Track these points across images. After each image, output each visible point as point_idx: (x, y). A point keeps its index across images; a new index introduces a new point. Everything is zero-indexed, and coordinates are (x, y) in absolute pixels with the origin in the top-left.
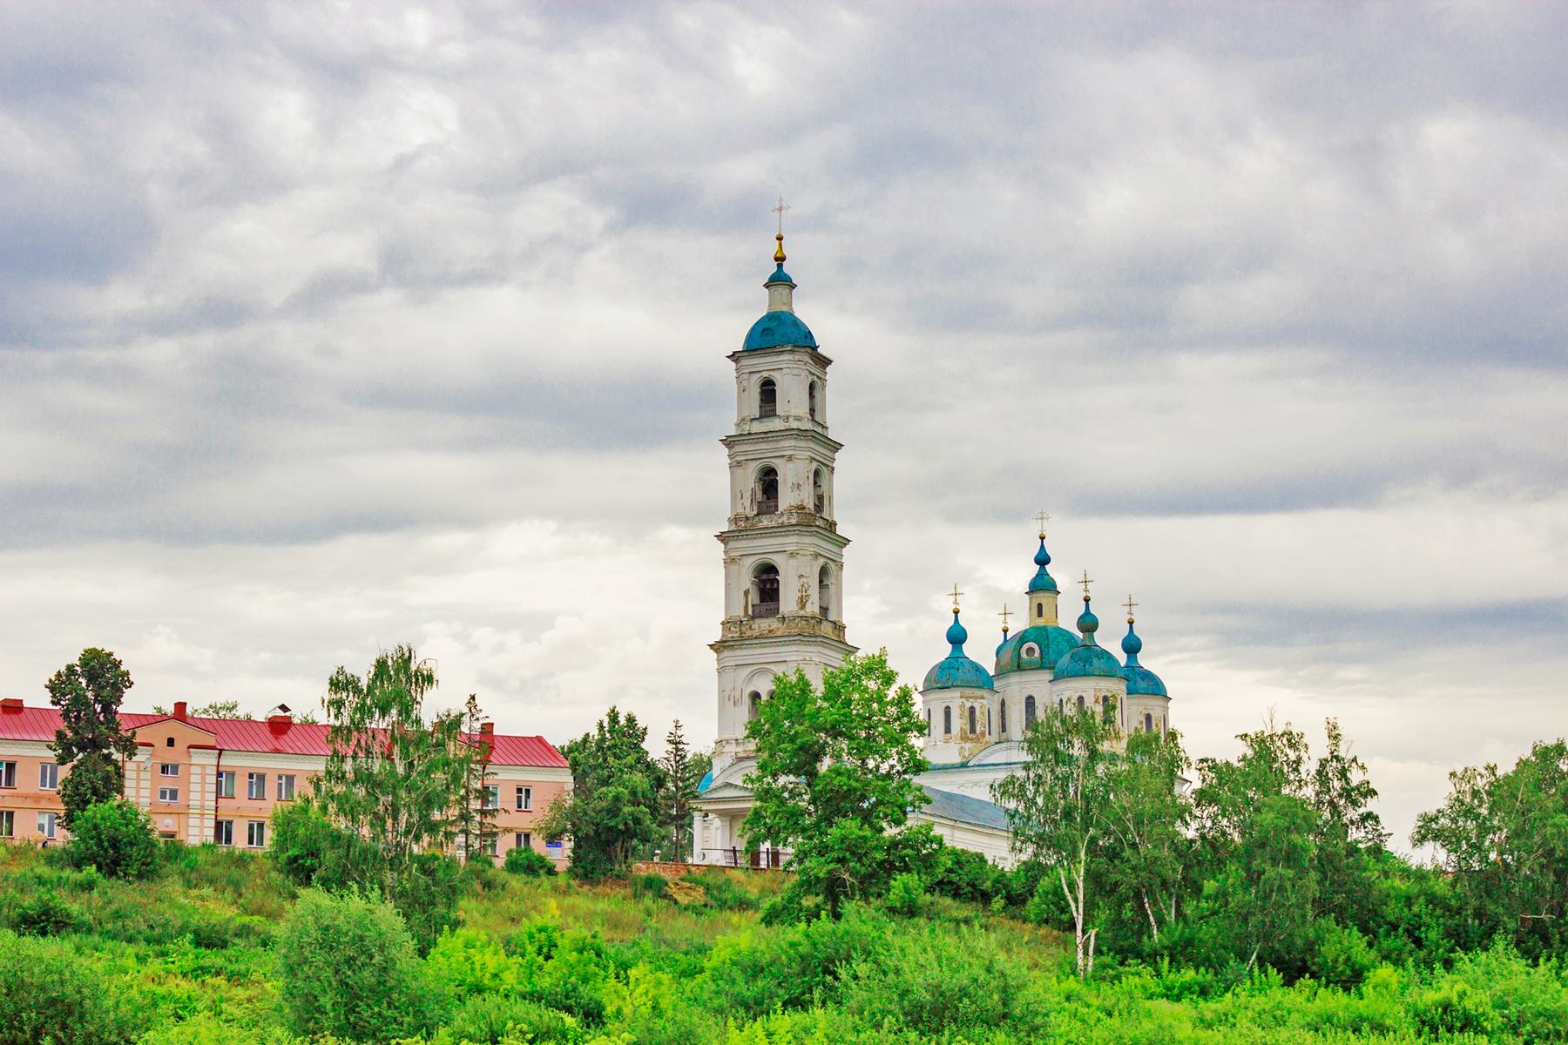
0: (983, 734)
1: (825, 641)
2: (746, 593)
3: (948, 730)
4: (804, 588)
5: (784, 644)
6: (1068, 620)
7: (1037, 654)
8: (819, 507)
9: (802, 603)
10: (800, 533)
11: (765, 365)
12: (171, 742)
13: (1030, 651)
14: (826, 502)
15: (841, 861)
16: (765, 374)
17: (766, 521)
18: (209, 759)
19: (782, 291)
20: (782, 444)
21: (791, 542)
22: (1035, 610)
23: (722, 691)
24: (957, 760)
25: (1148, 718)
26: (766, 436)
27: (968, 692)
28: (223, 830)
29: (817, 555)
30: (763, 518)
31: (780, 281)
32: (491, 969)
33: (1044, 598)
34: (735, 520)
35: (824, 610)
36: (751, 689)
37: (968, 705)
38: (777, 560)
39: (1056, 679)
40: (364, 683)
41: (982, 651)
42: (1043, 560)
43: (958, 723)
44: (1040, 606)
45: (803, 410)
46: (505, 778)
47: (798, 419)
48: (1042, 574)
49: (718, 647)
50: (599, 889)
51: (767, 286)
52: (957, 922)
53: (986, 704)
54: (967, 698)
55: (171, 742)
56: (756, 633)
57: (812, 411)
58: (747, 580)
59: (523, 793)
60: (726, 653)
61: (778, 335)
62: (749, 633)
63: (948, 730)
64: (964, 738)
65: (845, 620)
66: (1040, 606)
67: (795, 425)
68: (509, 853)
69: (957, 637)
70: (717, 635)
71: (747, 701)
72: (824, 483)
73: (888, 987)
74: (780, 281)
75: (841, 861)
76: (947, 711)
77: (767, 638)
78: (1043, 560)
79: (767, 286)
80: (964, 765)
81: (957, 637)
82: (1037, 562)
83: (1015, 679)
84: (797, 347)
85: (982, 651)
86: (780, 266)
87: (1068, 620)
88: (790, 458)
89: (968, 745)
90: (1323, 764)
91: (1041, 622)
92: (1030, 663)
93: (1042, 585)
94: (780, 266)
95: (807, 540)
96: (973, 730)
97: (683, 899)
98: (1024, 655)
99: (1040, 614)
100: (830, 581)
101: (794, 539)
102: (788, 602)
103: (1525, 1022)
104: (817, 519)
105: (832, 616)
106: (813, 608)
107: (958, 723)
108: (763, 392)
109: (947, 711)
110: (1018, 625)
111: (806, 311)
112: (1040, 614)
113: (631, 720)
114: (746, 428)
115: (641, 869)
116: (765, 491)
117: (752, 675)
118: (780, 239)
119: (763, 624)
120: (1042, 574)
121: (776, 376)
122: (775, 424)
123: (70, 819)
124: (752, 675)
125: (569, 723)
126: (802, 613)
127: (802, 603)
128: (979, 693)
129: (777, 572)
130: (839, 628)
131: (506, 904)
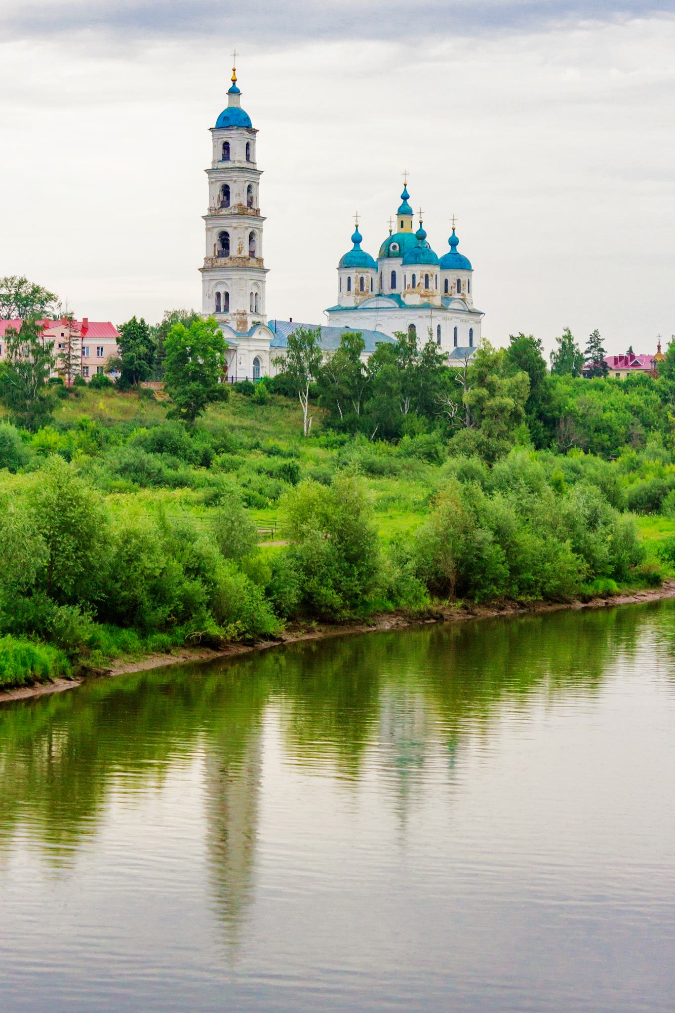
0: (367, 291)
1: (251, 269)
2: (215, 245)
3: (349, 289)
4: (241, 244)
5: (228, 271)
7: (398, 249)
8: (250, 203)
9: (240, 251)
10: (239, 218)
11: (226, 135)
13: (394, 247)
14: (254, 200)
15: (191, 398)
16: (225, 140)
17: (224, 211)
19: (235, 97)
20: (232, 174)
21: (235, 222)
23: (204, 291)
25: (459, 281)
26: (224, 170)
27: (360, 269)
29: (247, 228)
31: (234, 92)
32: (54, 441)
33: (404, 218)
34: (210, 210)
35: (252, 254)
37: (360, 276)
38: (229, 230)
40: (18, 331)
41: (372, 247)
42: (405, 197)
44: (402, 222)
45: (243, 158)
46: (91, 343)
47: (240, 162)
48: (405, 204)
49: (202, 270)
50: (126, 394)
52: (282, 406)
53: (369, 275)
54: (359, 273)
56: (219, 264)
57: (248, 156)
58: (215, 239)
59: (100, 350)
60: (205, 274)
61: (233, 121)
63: (349, 289)
64: (357, 294)
65: (264, 256)
66: (402, 222)
67: (238, 165)
68: (93, 376)
69: (357, 239)
71: (214, 296)
72: (253, 190)
74: (234, 92)
75: (191, 398)
76: (349, 279)
77: (223, 268)
78: (405, 197)
80: (356, 308)
81: (357, 239)
82: (402, 198)
83: (386, 261)
84: (239, 127)
85: (372, 247)
86: (234, 84)
88: (235, 181)
89: (359, 297)
90: (427, 345)
91: (402, 230)
94: (234, 84)
95: (242, 221)
96: (362, 289)
97: (159, 399)
98: (391, 249)
99: (402, 226)
100: (256, 238)
101: (235, 221)
102: (233, 251)
104: (250, 210)
105: (257, 255)
106: (246, 253)
107: (355, 286)
108: (224, 148)
109: (349, 279)
111: (245, 104)
112: (402, 226)
113: (142, 321)
114: (216, 166)
115: (144, 385)
116: (225, 195)
117: (217, 284)
119: (222, 260)
120: (405, 204)
121: (230, 141)
124: (217, 284)
125: (120, 320)
127: (240, 251)
128: (365, 270)
130: (260, 261)
131: (84, 404)
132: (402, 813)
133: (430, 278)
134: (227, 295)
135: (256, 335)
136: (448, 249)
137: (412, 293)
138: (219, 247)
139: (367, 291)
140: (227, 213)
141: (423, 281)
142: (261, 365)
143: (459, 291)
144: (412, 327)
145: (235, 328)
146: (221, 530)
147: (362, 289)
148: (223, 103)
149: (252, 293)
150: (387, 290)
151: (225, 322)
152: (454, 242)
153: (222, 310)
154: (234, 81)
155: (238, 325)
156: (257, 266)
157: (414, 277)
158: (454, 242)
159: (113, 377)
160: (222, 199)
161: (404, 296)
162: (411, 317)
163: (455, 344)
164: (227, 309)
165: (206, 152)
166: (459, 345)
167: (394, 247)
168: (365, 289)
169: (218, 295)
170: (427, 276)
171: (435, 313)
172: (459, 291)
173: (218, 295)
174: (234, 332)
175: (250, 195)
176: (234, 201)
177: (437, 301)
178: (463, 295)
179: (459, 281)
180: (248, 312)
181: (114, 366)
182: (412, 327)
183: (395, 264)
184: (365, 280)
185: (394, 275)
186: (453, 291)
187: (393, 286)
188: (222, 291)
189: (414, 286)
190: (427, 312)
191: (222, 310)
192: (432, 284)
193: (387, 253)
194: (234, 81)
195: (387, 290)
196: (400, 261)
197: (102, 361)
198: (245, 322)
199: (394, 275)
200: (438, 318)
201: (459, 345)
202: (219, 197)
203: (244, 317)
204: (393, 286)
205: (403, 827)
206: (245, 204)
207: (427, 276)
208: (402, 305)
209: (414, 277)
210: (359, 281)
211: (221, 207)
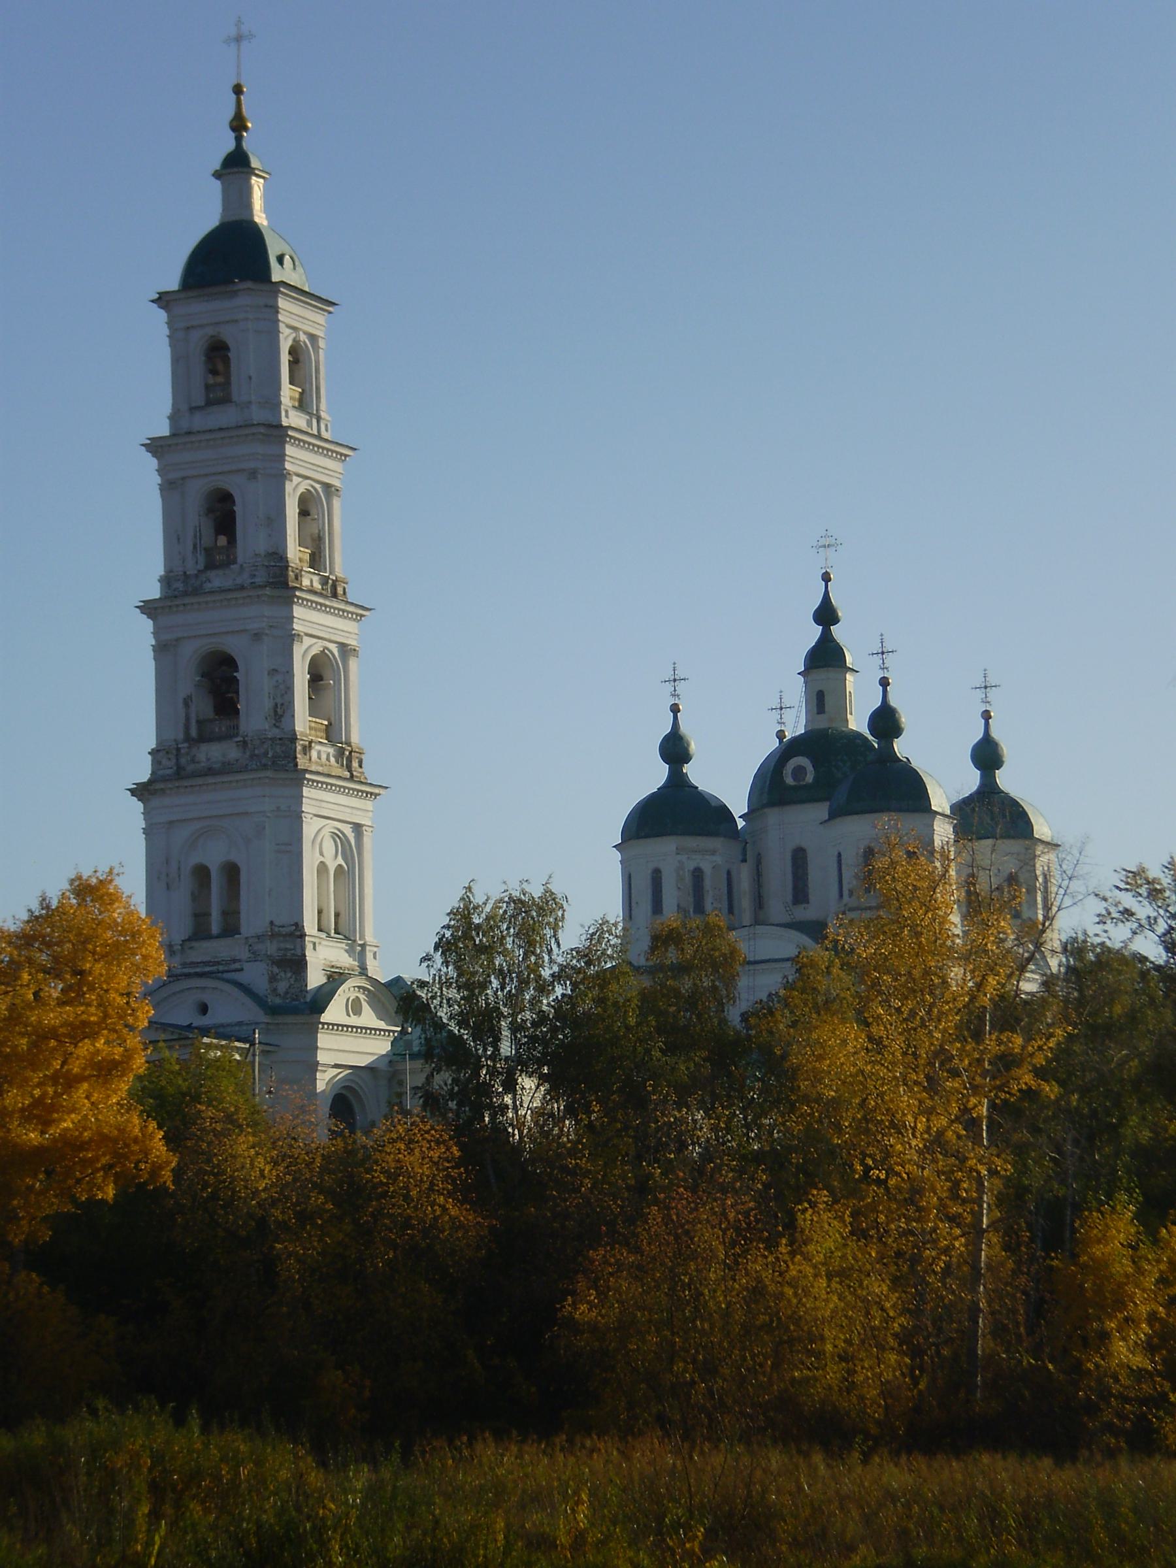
2: (187, 702)
6: (858, 722)
16: (210, 331)
17: (217, 580)
22: (829, 701)
30: (211, 574)
36: (196, 859)
37: (691, 865)
39: (834, 815)
41: (727, 775)
42: (826, 615)
51: (217, 175)
58: (188, 682)
60: (156, 802)
62: (191, 768)
69: (675, 750)
70: (144, 773)
73: (846, 1317)
78: (826, 615)
79: (217, 175)
81: (675, 750)
85: (727, 775)
87: (858, 722)
91: (822, 723)
93: (825, 658)
94: (239, 139)
98: (789, 781)
103: (287, 1502)
110: (796, 726)
119: (213, 753)
121: (228, 334)
122: (224, 416)
129: (235, 667)
132: (826, 598)
134: (232, 872)
136: (971, 780)
138: (204, 707)
140: (228, 583)
145: (261, 985)
148: (205, 214)
150: (778, 904)
152: (987, 756)
158: (987, 756)
160: (207, 541)
165: (144, 386)
183: (805, 823)
184: (707, 883)
185: (799, 858)
187: (800, 894)
188: (214, 856)
193: (773, 786)
196: (820, 811)
199: (799, 858)
204: (800, 894)
205: (777, 925)
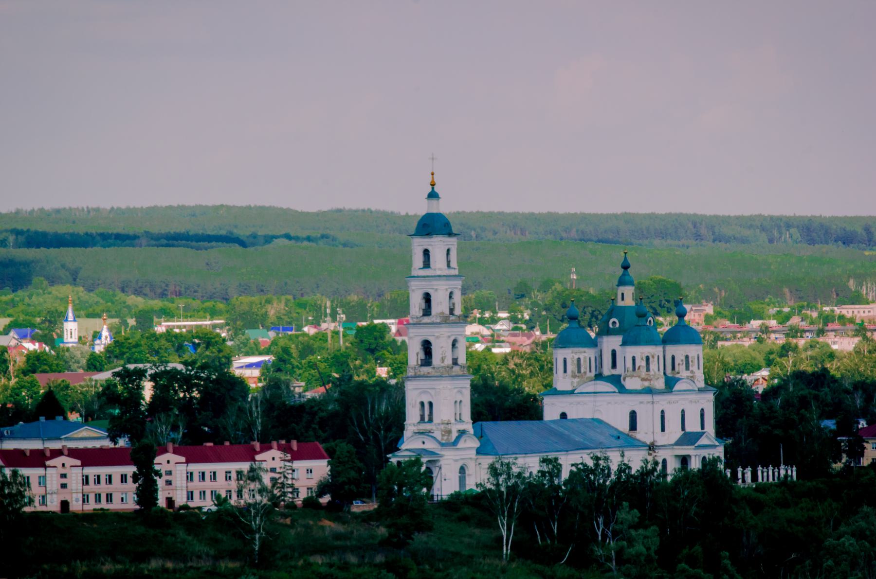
0: (585, 373)
2: (417, 354)
3: (565, 371)
7: (618, 325)
12: (168, 462)
16: (425, 247)
17: (426, 320)
18: (183, 467)
19: (434, 202)
21: (437, 331)
24: (570, 388)
25: (687, 357)
27: (576, 350)
28: (190, 495)
29: (449, 337)
31: (433, 195)
37: (576, 357)
38: (431, 339)
40: (246, 473)
43: (570, 368)
47: (440, 269)
55: (168, 462)
56: (422, 373)
63: (565, 371)
64: (574, 376)
71: (418, 406)
80: (572, 392)
86: (433, 188)
89: (576, 380)
92: (614, 329)
94: (433, 188)
96: (579, 371)
98: (611, 326)
102: (436, 360)
117: (421, 393)
118: (433, 174)
119: (426, 370)
121: (430, 248)
123: (25, 373)
124: (421, 393)
126: (442, 365)
127: (443, 360)
133: (651, 359)
134: (431, 404)
135: (461, 445)
137: (632, 376)
138: (422, 356)
139: (585, 373)
140: (429, 321)
141: (644, 363)
142: (467, 472)
143: (687, 368)
144: (633, 416)
145: (439, 438)
146: (622, 523)
147: (579, 371)
149: (456, 402)
151: (430, 432)
153: (426, 419)
154: (433, 185)
155: (443, 435)
156: (461, 373)
157: (634, 359)
159: (325, 499)
161: (624, 380)
162: (630, 403)
163: (683, 428)
164: (431, 420)
166: (688, 429)
167: (614, 323)
168: (582, 370)
169: (422, 404)
170: (648, 359)
171: (657, 398)
172: (687, 368)
173: (422, 404)
174: (439, 443)
175: (453, 301)
176: (435, 309)
177: (660, 384)
178: (692, 372)
179: (687, 357)
180: (453, 421)
181: (323, 488)
182: (633, 416)
185: (614, 354)
186: (681, 368)
187: (614, 365)
189: (634, 369)
190: (648, 398)
191: (426, 419)
192: (653, 366)
194: (433, 185)
195: (607, 371)
197: (314, 483)
198: (449, 432)
199: (614, 354)
200: (663, 402)
201: (688, 429)
202: (420, 304)
203: (449, 427)
204: (614, 365)
206: (447, 312)
207: (648, 359)
208: (622, 390)
209: (634, 359)
210: (576, 362)
211: (424, 315)
